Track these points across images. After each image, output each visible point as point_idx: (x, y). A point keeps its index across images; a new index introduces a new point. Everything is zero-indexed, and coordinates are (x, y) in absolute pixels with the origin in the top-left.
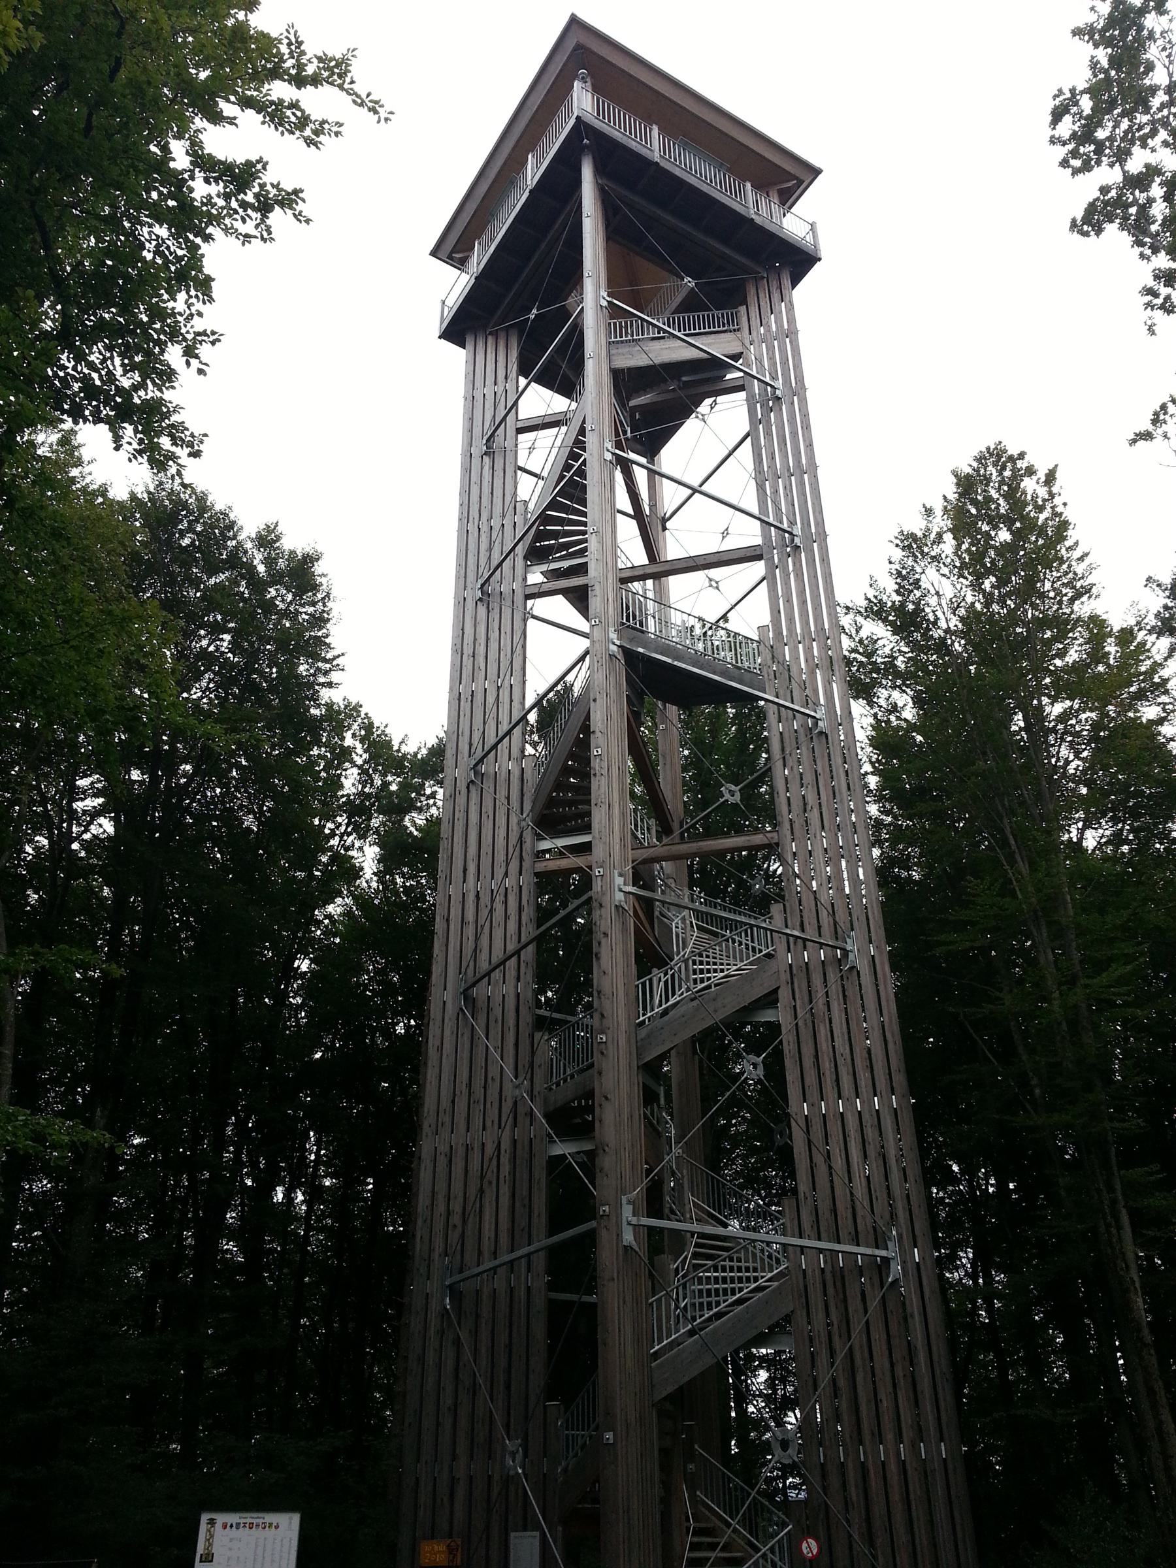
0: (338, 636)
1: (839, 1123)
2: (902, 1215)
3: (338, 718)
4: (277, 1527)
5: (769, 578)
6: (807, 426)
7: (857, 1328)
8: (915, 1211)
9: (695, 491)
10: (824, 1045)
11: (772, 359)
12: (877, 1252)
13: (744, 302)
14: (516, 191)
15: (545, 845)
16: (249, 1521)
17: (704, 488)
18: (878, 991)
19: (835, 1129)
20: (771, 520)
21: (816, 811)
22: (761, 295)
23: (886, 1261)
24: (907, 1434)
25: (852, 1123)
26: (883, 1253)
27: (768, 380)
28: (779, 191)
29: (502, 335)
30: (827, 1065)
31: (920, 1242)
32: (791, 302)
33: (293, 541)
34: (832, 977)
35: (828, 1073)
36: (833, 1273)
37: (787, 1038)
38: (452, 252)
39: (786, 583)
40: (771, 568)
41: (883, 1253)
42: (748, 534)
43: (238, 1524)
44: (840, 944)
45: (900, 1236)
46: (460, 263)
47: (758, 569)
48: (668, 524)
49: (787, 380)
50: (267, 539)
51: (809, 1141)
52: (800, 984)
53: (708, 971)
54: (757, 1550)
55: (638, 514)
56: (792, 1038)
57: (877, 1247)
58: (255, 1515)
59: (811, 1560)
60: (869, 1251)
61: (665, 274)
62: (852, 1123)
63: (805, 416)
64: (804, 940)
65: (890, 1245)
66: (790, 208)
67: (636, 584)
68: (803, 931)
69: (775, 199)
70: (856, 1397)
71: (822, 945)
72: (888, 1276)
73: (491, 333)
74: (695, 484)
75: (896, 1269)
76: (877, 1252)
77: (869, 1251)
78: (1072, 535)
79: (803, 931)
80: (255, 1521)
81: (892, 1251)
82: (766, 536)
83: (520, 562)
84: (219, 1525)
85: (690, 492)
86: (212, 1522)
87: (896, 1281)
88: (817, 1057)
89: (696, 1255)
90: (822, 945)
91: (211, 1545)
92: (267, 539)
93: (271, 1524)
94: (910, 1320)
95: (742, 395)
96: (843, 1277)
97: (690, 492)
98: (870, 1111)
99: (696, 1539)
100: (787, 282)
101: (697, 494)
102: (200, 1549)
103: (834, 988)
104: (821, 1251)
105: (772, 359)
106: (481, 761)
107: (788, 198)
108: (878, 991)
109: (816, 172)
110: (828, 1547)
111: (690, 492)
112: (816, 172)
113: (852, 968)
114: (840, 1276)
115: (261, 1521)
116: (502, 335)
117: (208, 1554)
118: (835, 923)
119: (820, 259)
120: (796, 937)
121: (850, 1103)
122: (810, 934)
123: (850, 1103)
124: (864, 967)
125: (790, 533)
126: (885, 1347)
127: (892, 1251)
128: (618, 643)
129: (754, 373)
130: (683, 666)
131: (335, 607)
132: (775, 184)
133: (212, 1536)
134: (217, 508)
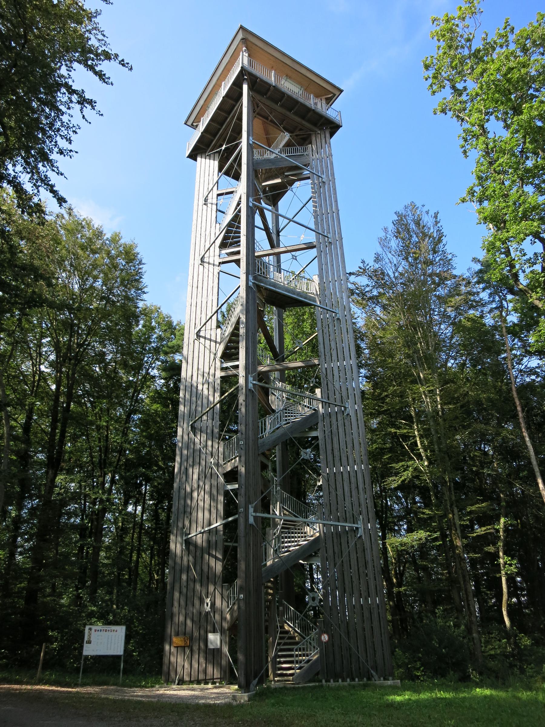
0: (145, 280)
1: (341, 476)
2: (364, 511)
3: (146, 313)
4: (116, 631)
5: (319, 256)
6: (335, 193)
7: (345, 554)
8: (369, 509)
9: (290, 220)
10: (336, 446)
11: (322, 166)
12: (354, 525)
13: (311, 143)
14: (217, 97)
15: (225, 365)
16: (105, 629)
17: (294, 219)
18: (358, 425)
19: (339, 478)
20: (320, 232)
21: (335, 350)
22: (318, 140)
23: (357, 528)
24: (364, 594)
25: (346, 476)
26: (356, 526)
27: (320, 175)
28: (326, 98)
29: (212, 156)
30: (336, 453)
31: (370, 520)
32: (330, 144)
33: (125, 240)
34: (339, 418)
35: (337, 456)
36: (336, 533)
37: (321, 442)
38: (193, 122)
39: (326, 258)
40: (320, 252)
41: (356, 526)
42: (311, 237)
43: (101, 630)
44: (343, 405)
45: (363, 519)
46: (194, 126)
47: (313, 252)
48: (280, 234)
49: (328, 176)
50: (115, 239)
51: (329, 485)
52: (327, 420)
53: (289, 416)
54: (304, 638)
55: (266, 229)
56: (323, 443)
57: (354, 523)
58: (108, 626)
59: (325, 643)
60: (350, 525)
61: (279, 132)
62: (346, 476)
63: (335, 189)
64: (329, 403)
65: (359, 522)
66: (331, 105)
67: (265, 258)
68: (329, 400)
69: (324, 102)
70: (344, 579)
71: (336, 405)
72: (358, 534)
73: (208, 155)
74: (291, 217)
75: (361, 532)
76: (354, 525)
77: (350, 525)
78: (444, 240)
79: (329, 400)
80: (108, 629)
81: (360, 525)
82: (318, 239)
83: (217, 249)
84: (93, 631)
85: (288, 221)
86: (90, 629)
87: (361, 536)
88: (333, 450)
89: (282, 528)
90: (336, 405)
91: (90, 637)
92: (115, 239)
93: (114, 630)
94: (366, 551)
95: (309, 181)
96: (340, 535)
97: (288, 221)
98: (353, 471)
99: (280, 641)
100: (328, 135)
101: (291, 222)
102: (86, 639)
103: (340, 423)
104: (332, 525)
105: (322, 166)
106: (200, 331)
107: (330, 101)
108: (358, 425)
109: (341, 91)
110: (331, 637)
111: (288, 221)
112: (341, 91)
113: (348, 414)
114: (339, 535)
115: (110, 629)
116: (212, 156)
117: (89, 641)
118: (342, 396)
119: (341, 126)
120: (326, 403)
121: (345, 468)
122: (332, 401)
123: (345, 468)
124: (352, 414)
125: (327, 237)
126: (356, 561)
127: (360, 525)
128: (253, 281)
129: (314, 172)
130: (280, 291)
131: (144, 268)
132: (324, 96)
133: (90, 634)
134: (96, 226)
